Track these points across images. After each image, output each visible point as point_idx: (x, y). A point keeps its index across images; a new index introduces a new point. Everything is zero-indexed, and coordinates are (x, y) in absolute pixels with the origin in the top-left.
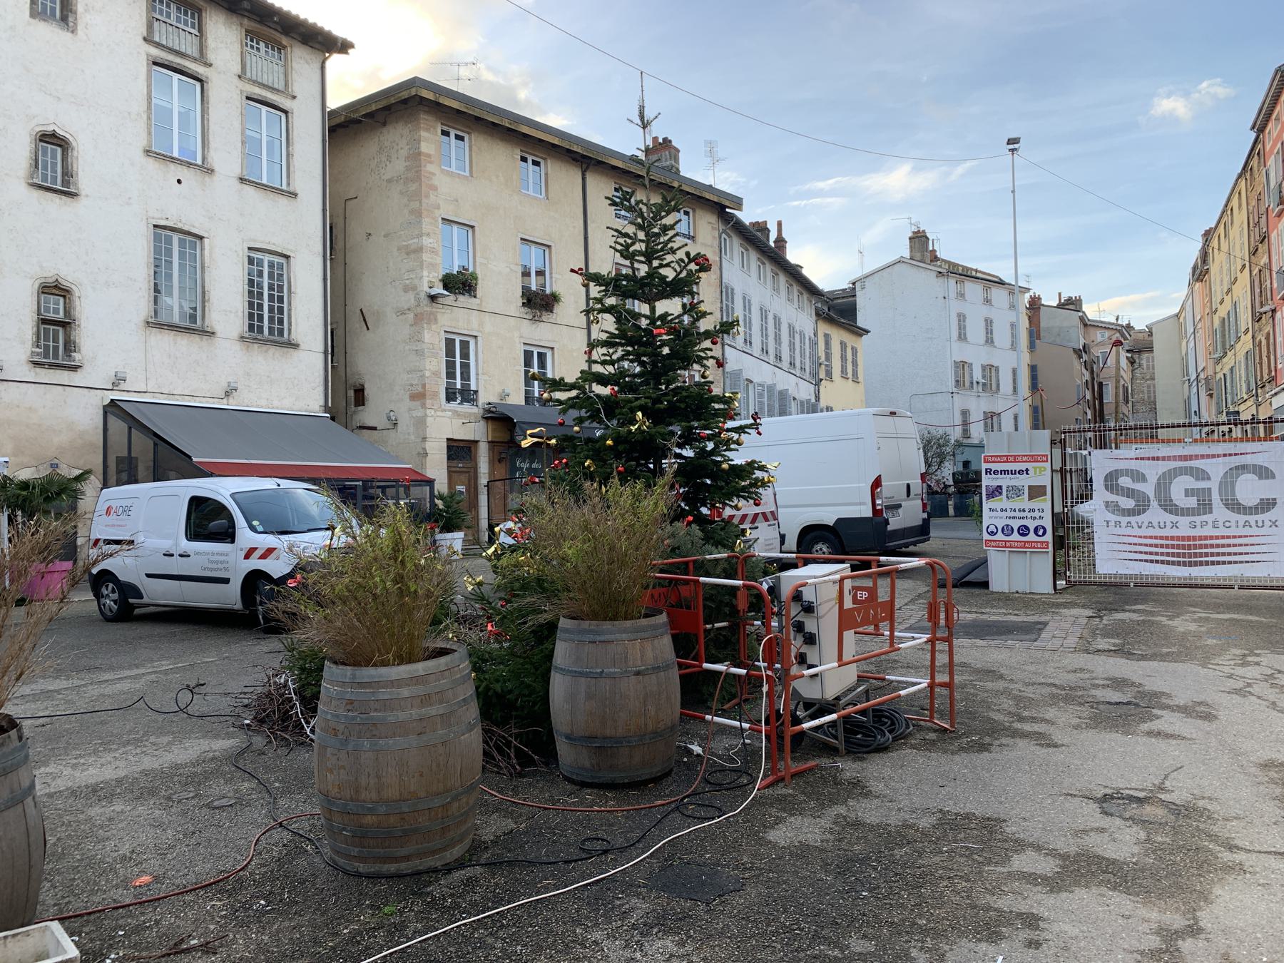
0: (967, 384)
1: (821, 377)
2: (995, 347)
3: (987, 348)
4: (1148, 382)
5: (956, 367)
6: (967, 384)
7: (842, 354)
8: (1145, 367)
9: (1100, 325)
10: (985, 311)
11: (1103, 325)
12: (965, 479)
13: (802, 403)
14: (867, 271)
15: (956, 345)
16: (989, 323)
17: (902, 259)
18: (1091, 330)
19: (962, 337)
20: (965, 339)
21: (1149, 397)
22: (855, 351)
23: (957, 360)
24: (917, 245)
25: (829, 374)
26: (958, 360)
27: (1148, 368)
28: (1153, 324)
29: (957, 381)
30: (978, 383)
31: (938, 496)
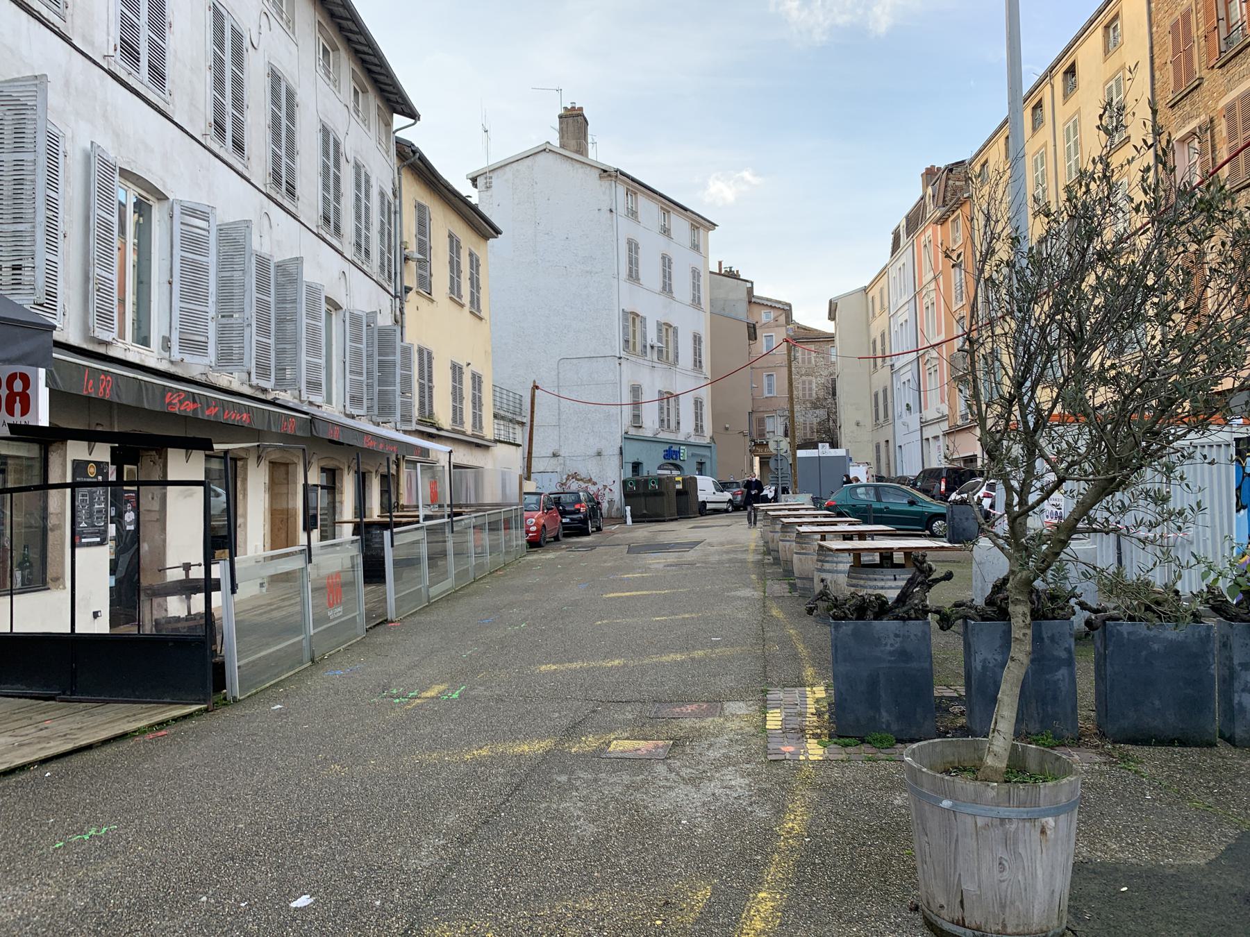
0: (639, 348)
1: (406, 283)
2: (673, 298)
3: (662, 299)
4: (804, 377)
5: (626, 320)
6: (639, 348)
7: (451, 258)
8: (800, 361)
9: (766, 303)
10: (661, 243)
11: (769, 304)
12: (641, 491)
13: (355, 320)
14: (495, 159)
15: (625, 286)
16: (666, 262)
17: (549, 147)
18: (755, 308)
19: (633, 276)
20: (638, 279)
21: (804, 395)
22: (475, 263)
23: (626, 310)
24: (571, 128)
25: (425, 283)
26: (628, 309)
27: (803, 362)
28: (839, 298)
29: (627, 341)
30: (652, 347)
31: (887, 626)
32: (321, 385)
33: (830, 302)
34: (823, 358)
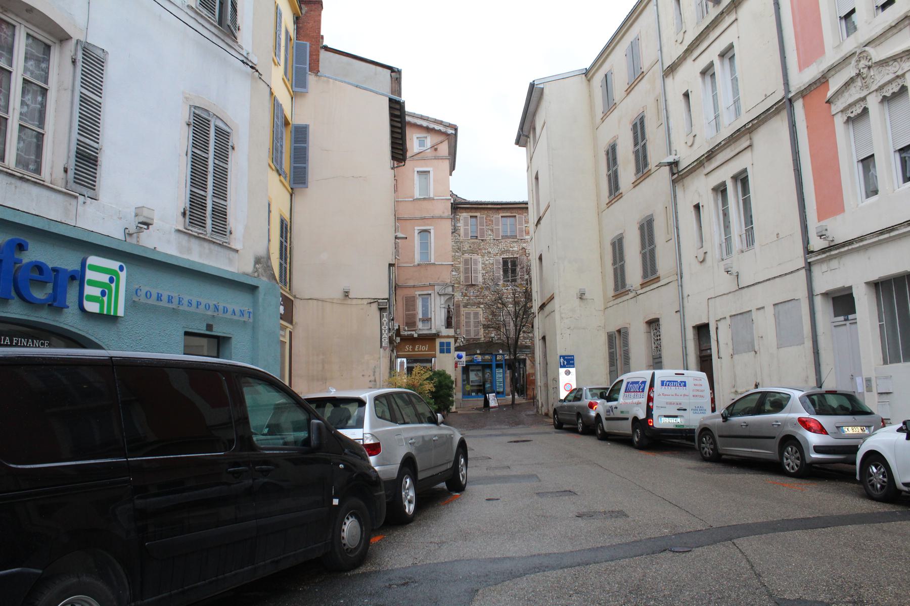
4: (467, 256)
9: (419, 122)
11: (425, 124)
32: (218, 357)
33: (532, 86)
34: (492, 230)
